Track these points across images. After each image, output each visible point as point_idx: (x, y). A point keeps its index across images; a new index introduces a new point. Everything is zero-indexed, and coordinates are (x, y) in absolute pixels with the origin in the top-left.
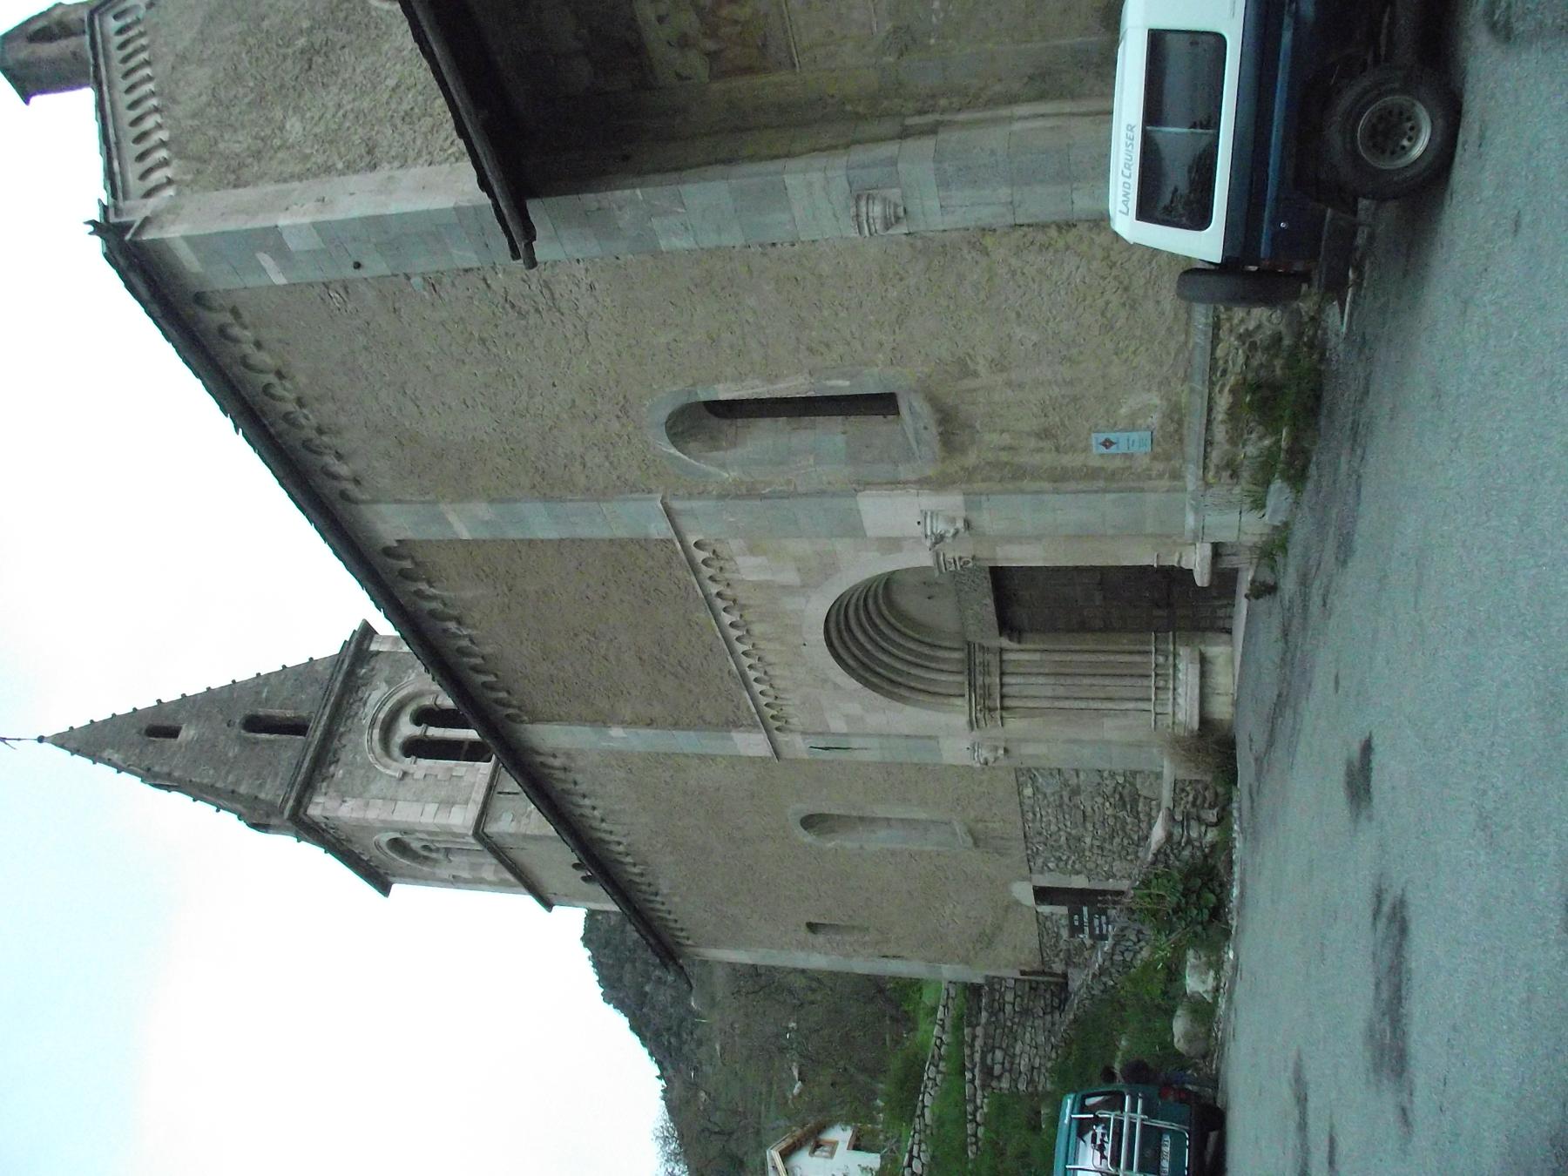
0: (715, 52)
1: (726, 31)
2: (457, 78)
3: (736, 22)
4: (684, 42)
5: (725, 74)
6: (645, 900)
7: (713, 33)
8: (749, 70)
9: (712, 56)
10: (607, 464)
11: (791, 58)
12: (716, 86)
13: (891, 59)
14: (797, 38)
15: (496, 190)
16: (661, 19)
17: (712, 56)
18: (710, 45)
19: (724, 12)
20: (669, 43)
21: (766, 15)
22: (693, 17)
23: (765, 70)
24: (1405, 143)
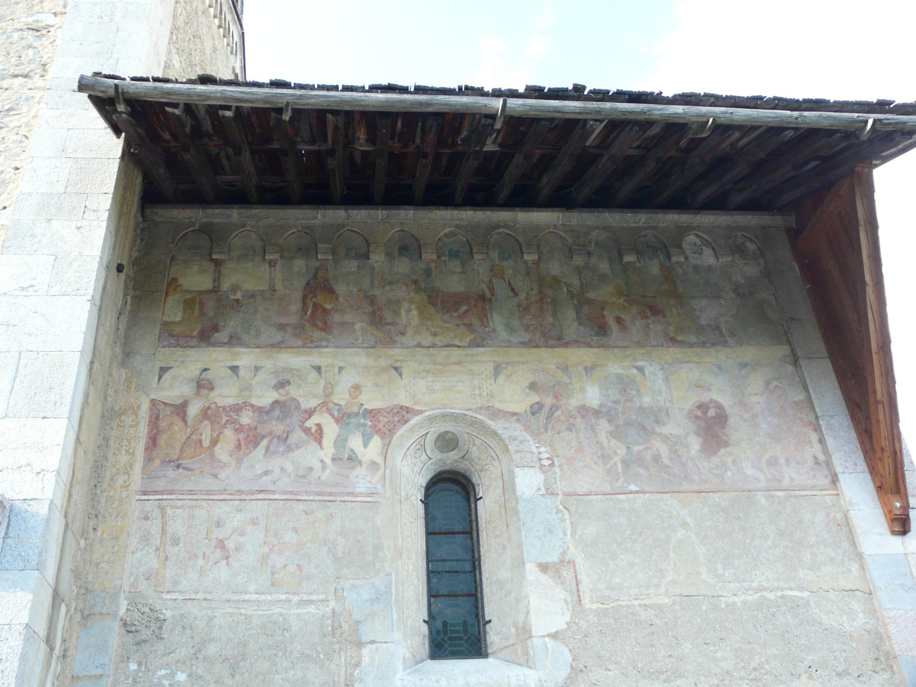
0: (185, 413)
1: (206, 432)
2: (381, 102)
3: (214, 442)
4: (203, 385)
5: (155, 420)
6: (732, 145)
7: (205, 414)
8: (153, 441)
9: (181, 409)
10: (43, 100)
11: (155, 492)
12: (145, 406)
13: (122, 611)
14: (180, 503)
15: (679, 109)
16: (235, 369)
17: (181, 409)
18: (193, 410)
19: (229, 433)
20: (205, 370)
21: (215, 476)
22: (230, 401)
23: (149, 459)
24: (286, 117)
